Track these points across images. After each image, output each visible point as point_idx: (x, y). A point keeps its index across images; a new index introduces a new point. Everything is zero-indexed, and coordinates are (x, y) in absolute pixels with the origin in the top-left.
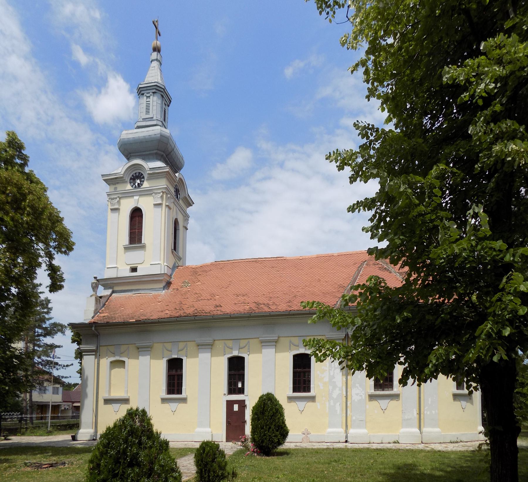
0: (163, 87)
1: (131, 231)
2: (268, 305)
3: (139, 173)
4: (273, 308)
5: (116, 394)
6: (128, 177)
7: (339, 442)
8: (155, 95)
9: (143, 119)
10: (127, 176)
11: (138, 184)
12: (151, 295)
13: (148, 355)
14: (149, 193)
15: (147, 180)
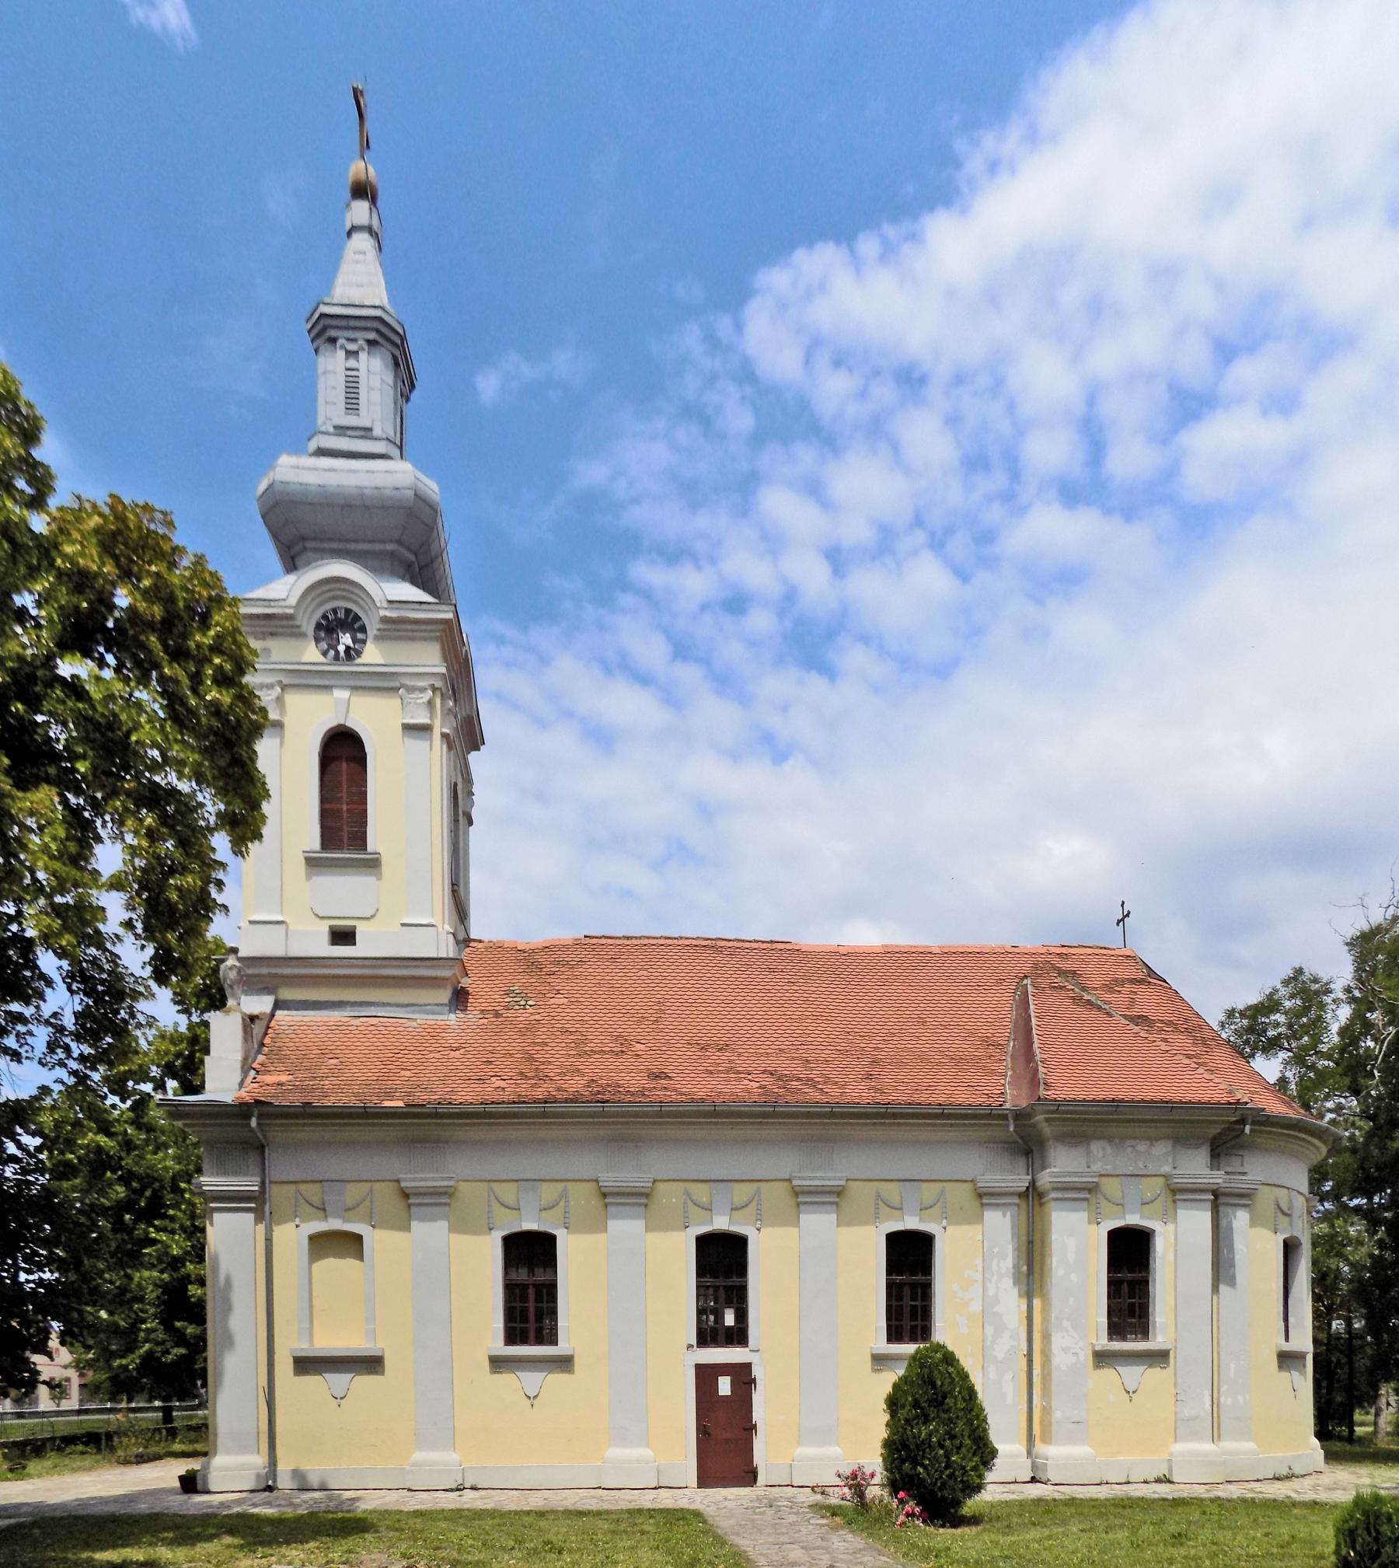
0: (402, 332)
1: (327, 806)
2: (810, 1082)
3: (348, 611)
4: (834, 1092)
5: (328, 1341)
6: (308, 623)
7: (1016, 1482)
8: (376, 350)
9: (335, 427)
10: (307, 615)
11: (348, 648)
12: (414, 1024)
13: (442, 1219)
14: (383, 683)
15: (377, 638)
